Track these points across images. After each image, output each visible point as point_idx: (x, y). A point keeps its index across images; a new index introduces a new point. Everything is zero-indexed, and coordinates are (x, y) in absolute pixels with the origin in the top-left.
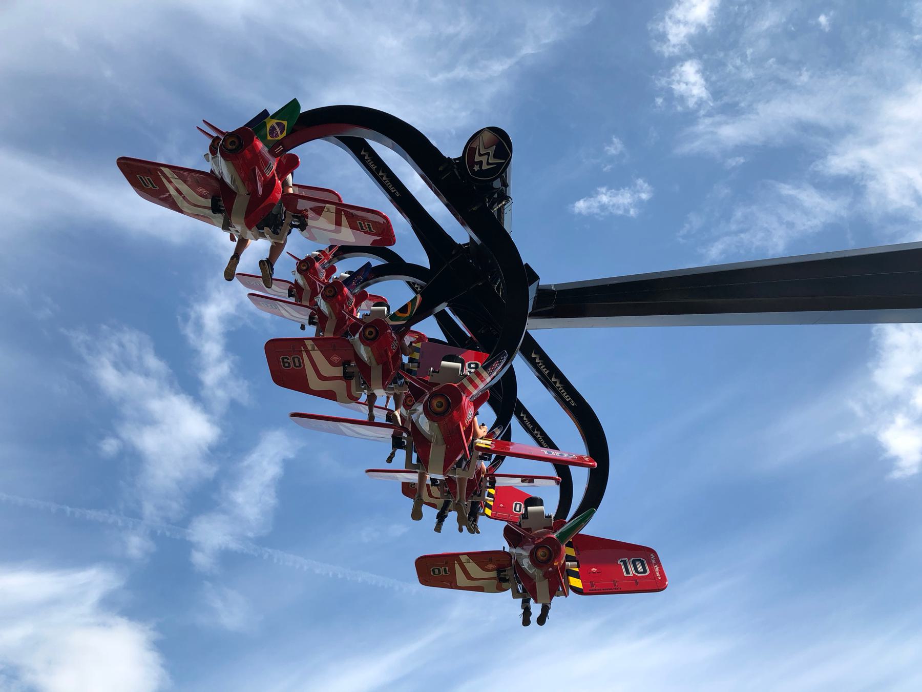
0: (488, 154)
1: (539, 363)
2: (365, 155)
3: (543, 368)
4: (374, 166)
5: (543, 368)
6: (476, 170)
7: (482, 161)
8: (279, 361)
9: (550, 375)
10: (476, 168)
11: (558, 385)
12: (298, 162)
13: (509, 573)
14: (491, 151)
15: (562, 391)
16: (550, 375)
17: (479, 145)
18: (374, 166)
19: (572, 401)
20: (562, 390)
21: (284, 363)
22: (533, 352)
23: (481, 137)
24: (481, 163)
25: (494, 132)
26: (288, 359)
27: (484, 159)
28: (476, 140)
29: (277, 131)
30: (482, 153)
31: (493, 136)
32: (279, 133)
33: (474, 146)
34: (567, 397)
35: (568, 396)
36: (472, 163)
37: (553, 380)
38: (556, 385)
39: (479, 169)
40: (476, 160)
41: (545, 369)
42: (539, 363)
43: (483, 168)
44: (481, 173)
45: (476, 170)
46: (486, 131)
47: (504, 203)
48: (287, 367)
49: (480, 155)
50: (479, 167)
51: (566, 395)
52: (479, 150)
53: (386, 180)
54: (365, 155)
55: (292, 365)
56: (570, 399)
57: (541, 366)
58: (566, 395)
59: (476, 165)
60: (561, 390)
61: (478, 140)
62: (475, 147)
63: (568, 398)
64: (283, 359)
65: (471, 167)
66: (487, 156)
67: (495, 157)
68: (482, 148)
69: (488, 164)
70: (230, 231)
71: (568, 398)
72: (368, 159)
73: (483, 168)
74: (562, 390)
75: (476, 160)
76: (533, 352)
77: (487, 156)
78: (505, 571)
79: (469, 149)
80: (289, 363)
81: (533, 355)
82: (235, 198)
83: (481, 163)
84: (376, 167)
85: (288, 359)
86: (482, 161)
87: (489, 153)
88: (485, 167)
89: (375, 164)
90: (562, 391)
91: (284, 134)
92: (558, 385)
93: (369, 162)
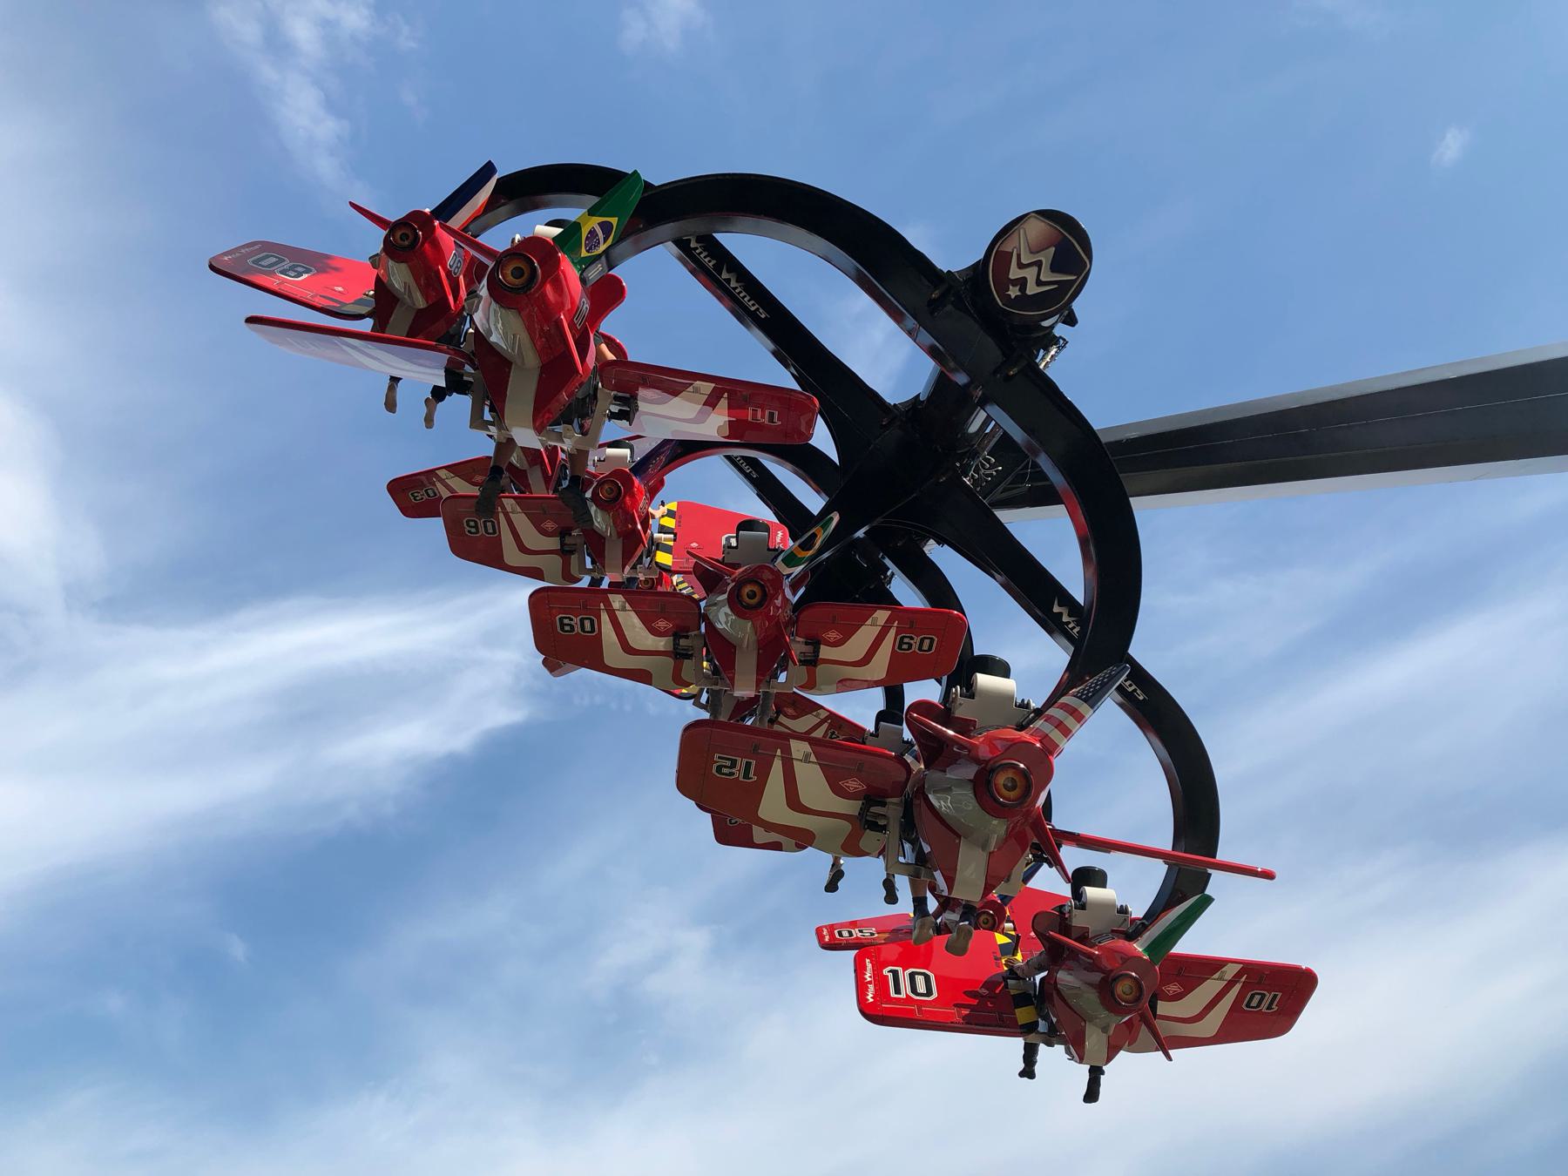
0: (1039, 264)
1: (1069, 623)
2: (1061, 614)
3: (705, 257)
4: (710, 261)
5: (705, 257)
6: (1013, 297)
7: (1024, 279)
8: (553, 624)
9: (718, 268)
10: (1014, 292)
11: (733, 284)
12: (623, 287)
13: (892, 811)
14: (1046, 257)
15: (741, 295)
16: (718, 268)
17: (1019, 245)
18: (710, 261)
19: (761, 310)
20: (740, 292)
21: (562, 625)
22: (1056, 602)
23: (1022, 231)
24: (1022, 283)
25: (1048, 218)
26: (571, 620)
27: (1030, 274)
28: (1013, 236)
29: (598, 239)
30: (1024, 261)
31: (1049, 227)
32: (602, 240)
33: (1007, 247)
34: (750, 303)
35: (752, 302)
36: (1004, 282)
37: (725, 275)
38: (729, 284)
39: (1019, 294)
40: (1012, 276)
41: (708, 259)
42: (1069, 623)
43: (1029, 292)
44: (1025, 301)
45: (1013, 297)
46: (1032, 219)
47: (1053, 353)
48: (472, 521)
49: (1021, 266)
50: (1020, 290)
51: (749, 301)
52: (1019, 256)
53: (736, 288)
54: (1061, 614)
55: (578, 629)
56: (757, 306)
57: (701, 253)
58: (749, 301)
59: (1013, 286)
60: (699, 254)
61: (1015, 235)
62: (1011, 250)
63: (753, 305)
64: (561, 619)
65: (1003, 290)
66: (1035, 269)
67: (1054, 268)
68: (1025, 248)
69: (1039, 283)
70: (490, 431)
71: (1130, 685)
72: (697, 248)
73: (1029, 292)
74: (740, 292)
75: (1012, 276)
76: (1056, 602)
77: (1035, 269)
78: (884, 804)
79: (997, 253)
80: (468, 525)
81: (1056, 609)
82: (510, 372)
83: (1022, 283)
84: (714, 262)
85: (571, 620)
86: (1024, 279)
87: (1041, 261)
88: (1032, 289)
89: (711, 255)
90: (741, 295)
91: (610, 241)
92: (733, 284)
93: (699, 254)
